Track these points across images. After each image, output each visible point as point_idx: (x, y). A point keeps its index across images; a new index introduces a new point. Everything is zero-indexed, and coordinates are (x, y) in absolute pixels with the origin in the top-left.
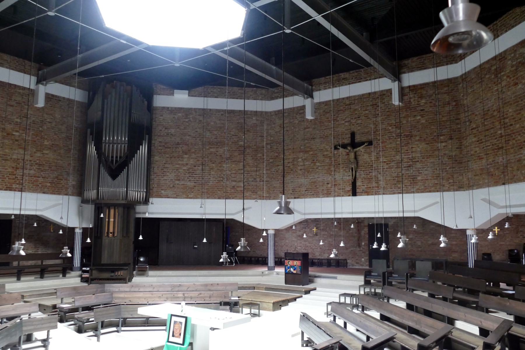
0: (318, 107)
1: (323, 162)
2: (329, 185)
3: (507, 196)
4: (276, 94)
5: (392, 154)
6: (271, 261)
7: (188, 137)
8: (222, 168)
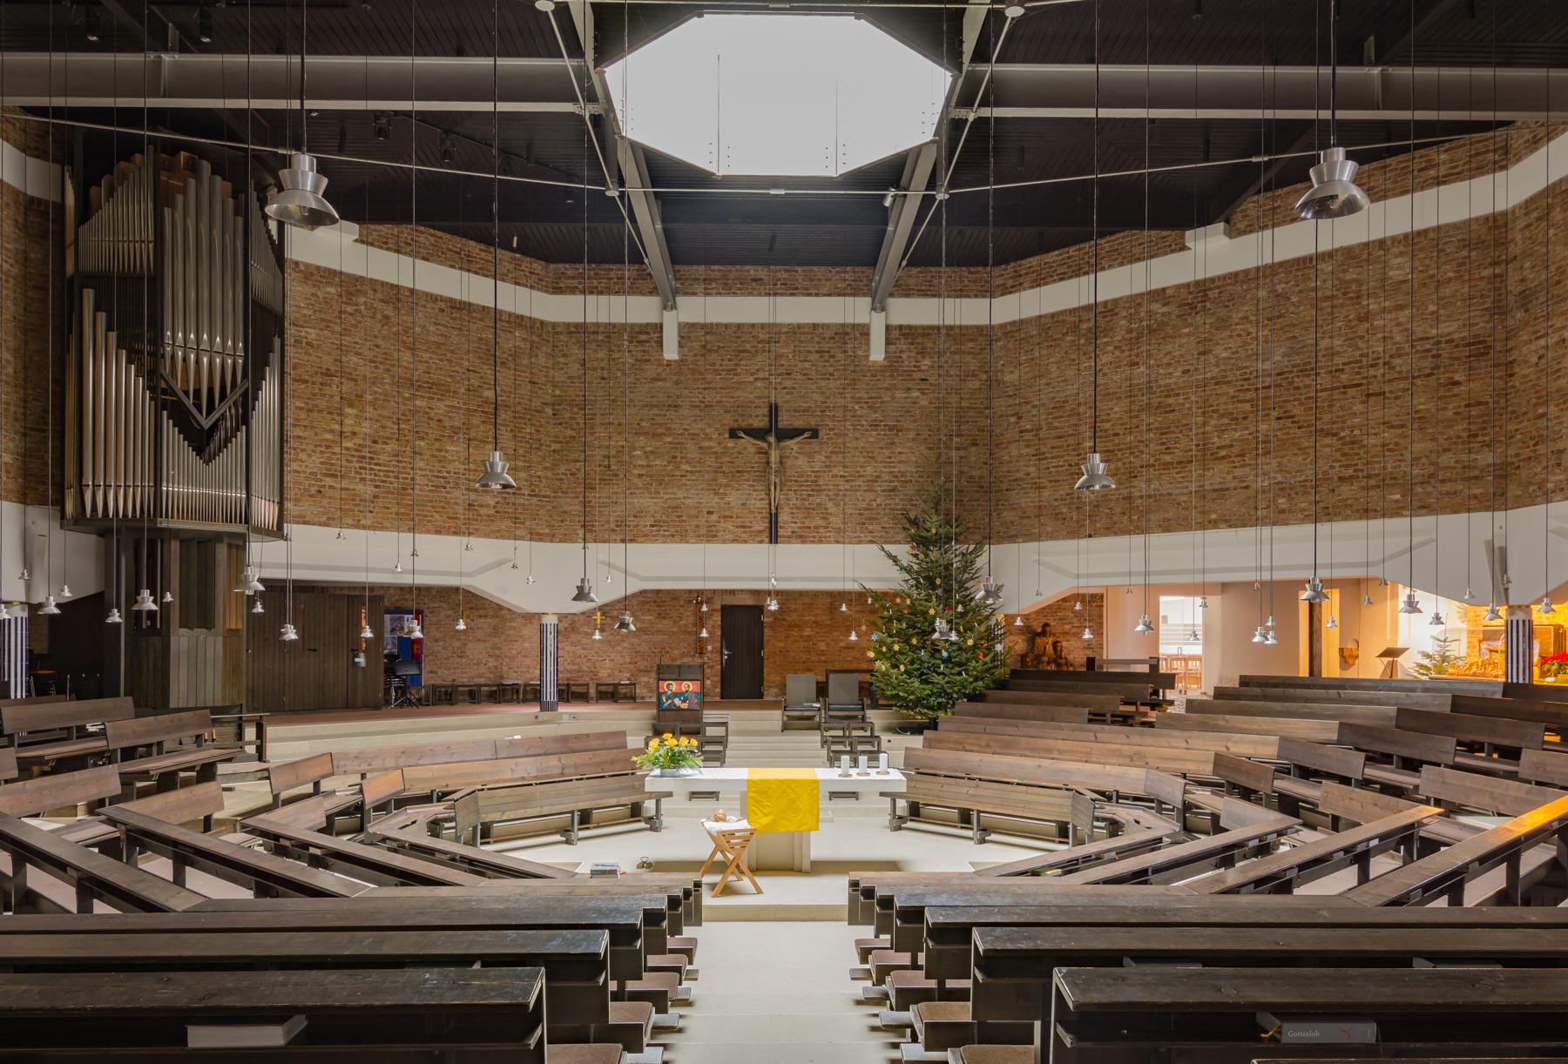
0: (688, 332)
1: (699, 462)
2: (714, 517)
3: (1258, 565)
4: (570, 281)
5: (858, 462)
6: (550, 693)
7: (355, 359)
8: (443, 454)
